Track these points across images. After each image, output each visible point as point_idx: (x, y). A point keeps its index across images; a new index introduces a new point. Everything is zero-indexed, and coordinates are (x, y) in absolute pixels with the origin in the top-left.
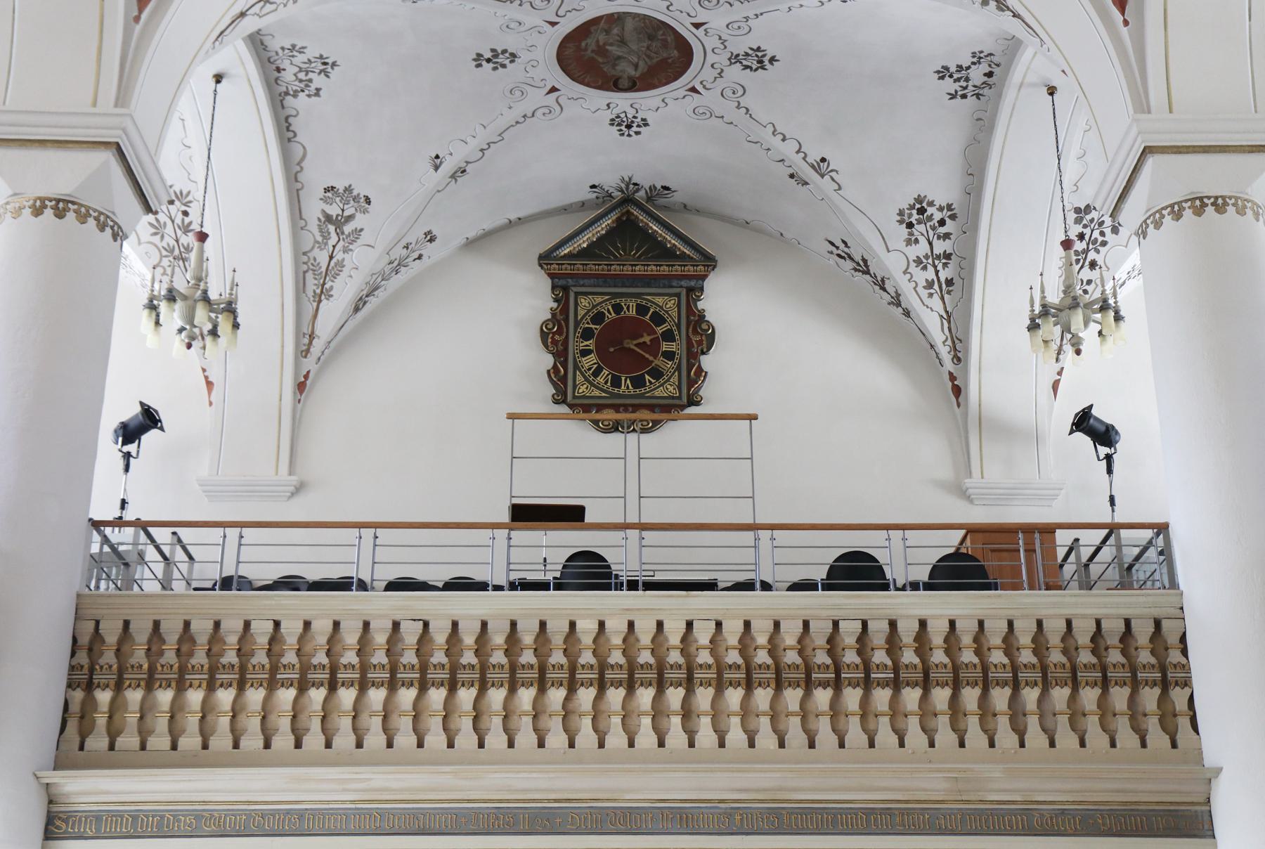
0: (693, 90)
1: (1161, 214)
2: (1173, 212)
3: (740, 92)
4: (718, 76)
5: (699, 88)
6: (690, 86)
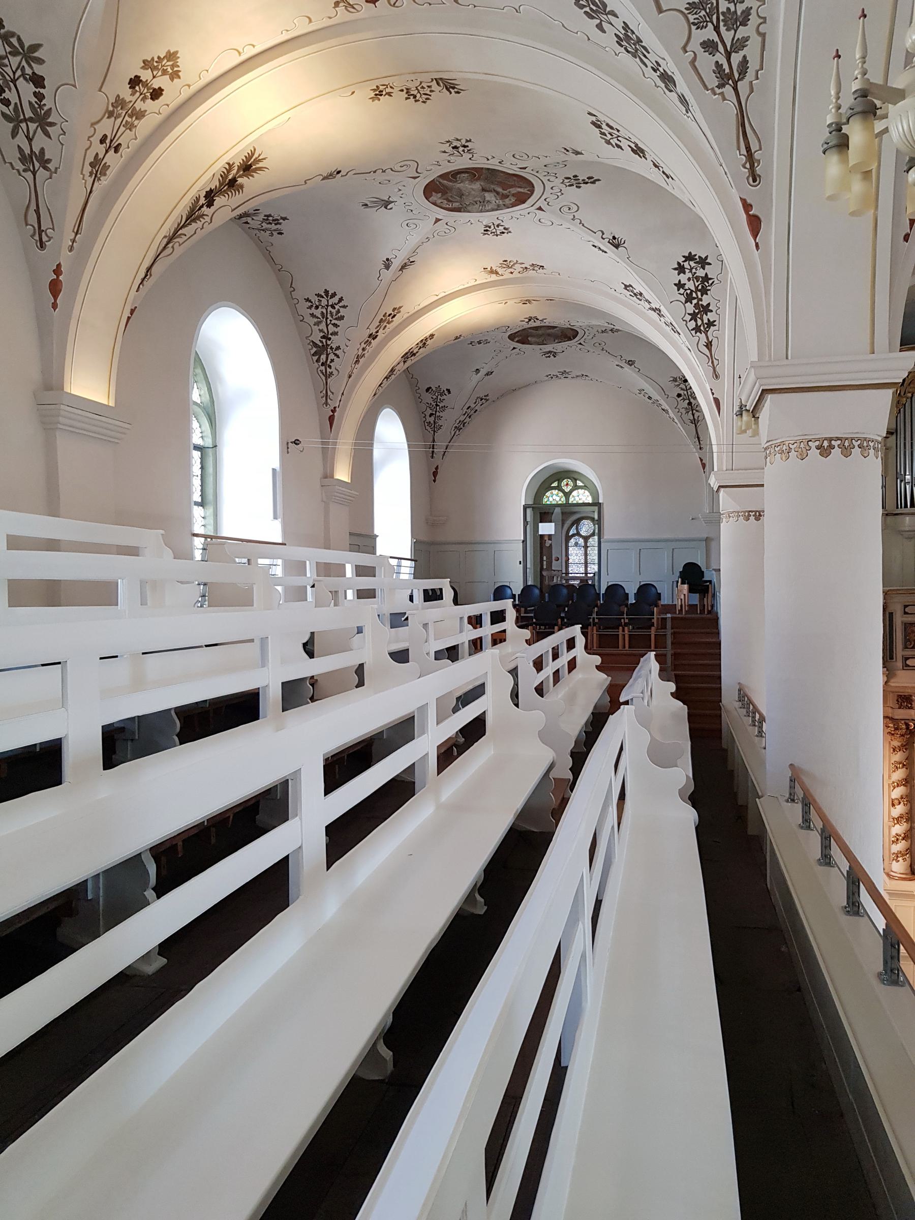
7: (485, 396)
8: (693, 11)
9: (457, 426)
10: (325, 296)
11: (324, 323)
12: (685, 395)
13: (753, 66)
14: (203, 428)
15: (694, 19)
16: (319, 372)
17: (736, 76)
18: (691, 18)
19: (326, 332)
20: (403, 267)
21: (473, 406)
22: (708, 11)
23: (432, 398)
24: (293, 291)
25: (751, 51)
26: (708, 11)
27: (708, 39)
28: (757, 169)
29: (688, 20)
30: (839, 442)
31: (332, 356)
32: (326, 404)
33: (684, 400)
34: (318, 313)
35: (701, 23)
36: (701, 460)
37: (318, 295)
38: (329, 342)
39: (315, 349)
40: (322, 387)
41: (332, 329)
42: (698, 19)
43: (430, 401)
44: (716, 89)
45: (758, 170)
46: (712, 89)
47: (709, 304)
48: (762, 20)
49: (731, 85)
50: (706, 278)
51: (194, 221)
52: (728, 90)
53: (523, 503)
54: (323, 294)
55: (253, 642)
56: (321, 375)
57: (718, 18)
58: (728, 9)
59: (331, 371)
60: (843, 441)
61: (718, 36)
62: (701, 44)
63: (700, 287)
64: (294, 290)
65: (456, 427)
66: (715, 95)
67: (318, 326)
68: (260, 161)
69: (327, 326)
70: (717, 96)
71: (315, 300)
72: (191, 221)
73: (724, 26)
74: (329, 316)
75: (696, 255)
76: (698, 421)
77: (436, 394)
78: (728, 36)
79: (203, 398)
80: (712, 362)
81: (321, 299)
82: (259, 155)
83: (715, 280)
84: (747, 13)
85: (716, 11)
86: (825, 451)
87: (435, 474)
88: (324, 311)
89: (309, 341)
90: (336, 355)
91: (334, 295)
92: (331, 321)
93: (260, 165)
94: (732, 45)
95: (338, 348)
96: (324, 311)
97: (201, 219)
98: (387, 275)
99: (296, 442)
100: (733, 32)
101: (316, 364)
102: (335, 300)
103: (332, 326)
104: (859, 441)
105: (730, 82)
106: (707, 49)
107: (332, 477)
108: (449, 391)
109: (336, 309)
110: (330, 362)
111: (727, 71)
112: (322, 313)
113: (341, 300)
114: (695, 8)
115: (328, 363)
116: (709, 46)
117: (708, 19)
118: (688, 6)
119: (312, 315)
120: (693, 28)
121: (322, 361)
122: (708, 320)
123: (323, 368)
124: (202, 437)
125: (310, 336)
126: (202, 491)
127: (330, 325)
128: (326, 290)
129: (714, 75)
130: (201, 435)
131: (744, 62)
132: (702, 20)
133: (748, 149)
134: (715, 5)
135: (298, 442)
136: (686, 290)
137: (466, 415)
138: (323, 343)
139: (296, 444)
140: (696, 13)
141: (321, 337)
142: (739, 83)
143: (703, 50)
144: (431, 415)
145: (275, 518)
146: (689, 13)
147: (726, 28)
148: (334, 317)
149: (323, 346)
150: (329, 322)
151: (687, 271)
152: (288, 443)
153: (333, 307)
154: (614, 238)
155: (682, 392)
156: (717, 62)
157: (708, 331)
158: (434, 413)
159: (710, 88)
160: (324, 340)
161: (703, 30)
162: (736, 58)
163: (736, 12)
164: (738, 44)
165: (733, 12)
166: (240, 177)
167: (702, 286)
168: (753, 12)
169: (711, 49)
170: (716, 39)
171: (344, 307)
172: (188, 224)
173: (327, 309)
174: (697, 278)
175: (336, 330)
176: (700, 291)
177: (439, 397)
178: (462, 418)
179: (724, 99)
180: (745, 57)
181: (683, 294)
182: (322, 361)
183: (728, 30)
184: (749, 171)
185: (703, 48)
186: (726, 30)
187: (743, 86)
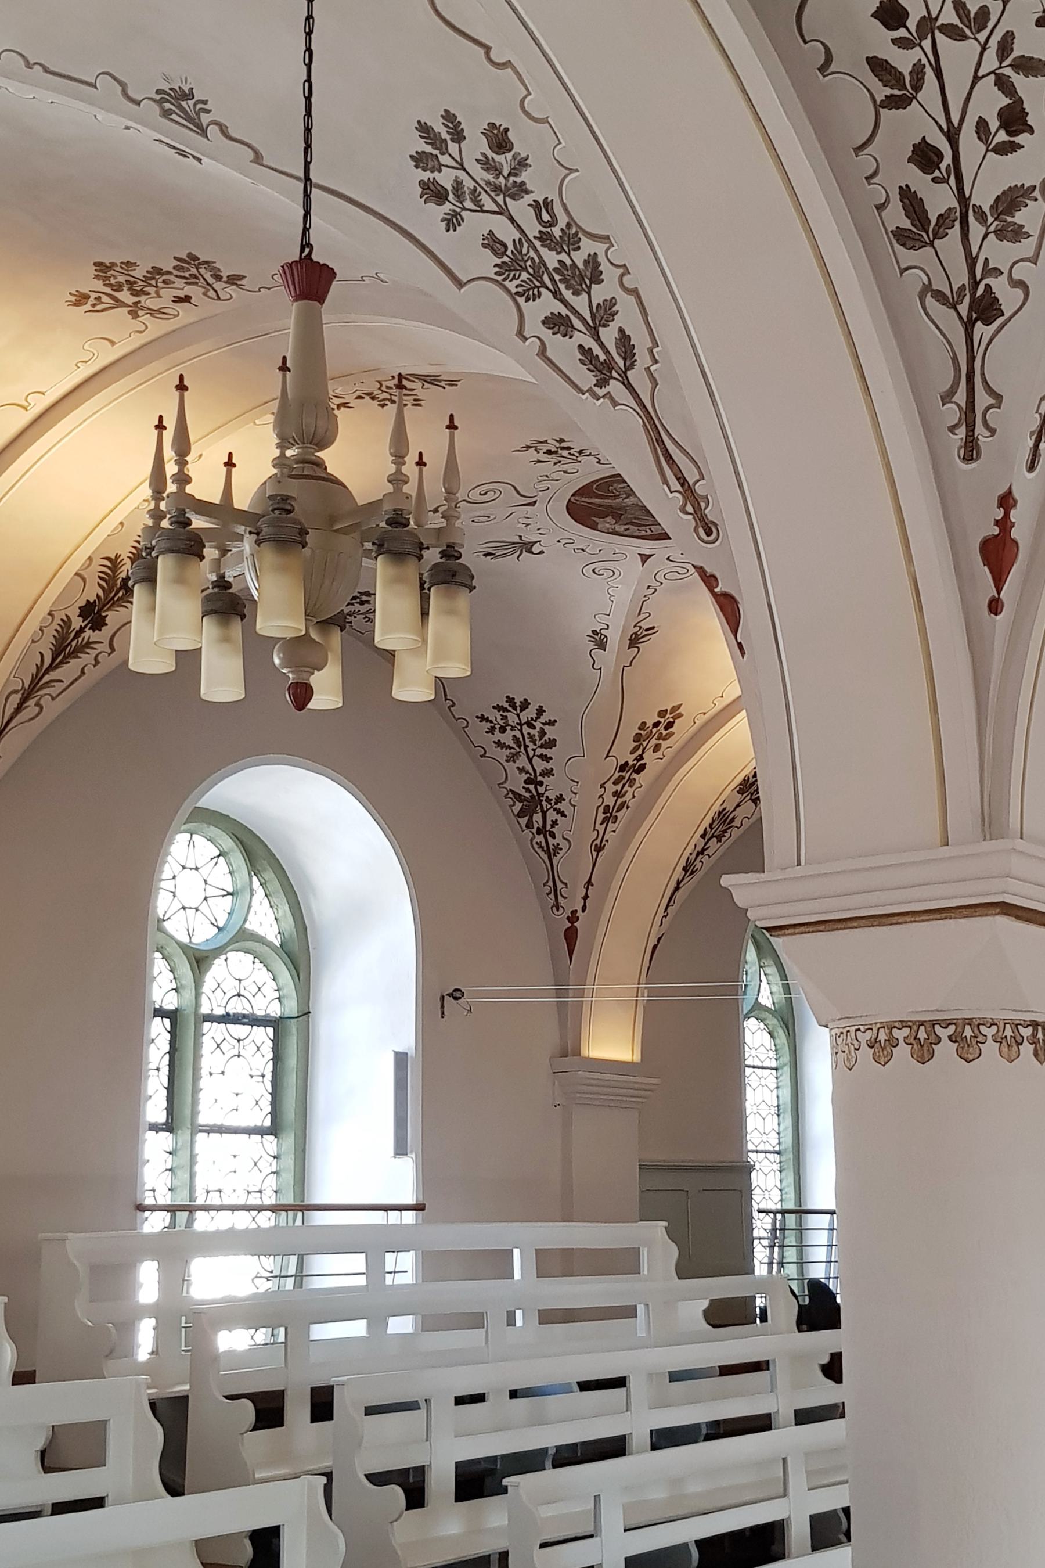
8: (509, 275)
10: (510, 708)
11: (524, 757)
14: (281, 981)
15: (517, 287)
16: (536, 846)
17: (620, 362)
18: (512, 286)
19: (531, 771)
20: (635, 641)
22: (531, 271)
24: (452, 706)
25: (627, 317)
26: (531, 271)
27: (552, 313)
28: (706, 512)
30: (906, 1032)
31: (552, 815)
35: (528, 290)
37: (499, 708)
38: (541, 790)
41: (540, 765)
42: (522, 286)
44: (596, 389)
45: (710, 513)
46: (590, 390)
48: (621, 270)
49: (617, 379)
51: (74, 654)
52: (615, 387)
54: (506, 705)
55: (456, 1398)
56: (539, 851)
57: (552, 279)
59: (555, 842)
60: (915, 1028)
61: (566, 306)
62: (544, 323)
66: (598, 400)
67: (514, 762)
69: (530, 760)
70: (602, 400)
71: (495, 716)
72: (65, 657)
73: (567, 288)
78: (580, 303)
79: (283, 925)
81: (505, 714)
85: (543, 269)
86: (924, 1052)
88: (518, 734)
89: (505, 792)
90: (558, 811)
91: (525, 705)
92: (534, 750)
95: (560, 799)
96: (518, 734)
97: (88, 651)
98: (609, 658)
99: (457, 995)
100: (585, 296)
101: (527, 831)
102: (530, 713)
103: (540, 760)
104: (952, 1028)
105: (614, 374)
106: (556, 329)
107: (577, 1052)
109: (538, 729)
110: (552, 826)
111: (602, 357)
113: (540, 711)
114: (511, 270)
115: (548, 827)
116: (557, 323)
117: (538, 284)
118: (497, 269)
119: (499, 744)
120: (521, 300)
123: (540, 838)
124: (279, 999)
125: (505, 782)
126: (273, 1103)
127: (535, 757)
128: (508, 697)
129: (585, 367)
130: (276, 995)
131: (624, 338)
132: (529, 287)
133: (682, 480)
134: (537, 260)
135: (458, 994)
138: (530, 792)
139: (456, 998)
140: (514, 278)
141: (525, 782)
142: (629, 373)
143: (551, 331)
145: (401, 1149)
146: (505, 280)
147: (571, 291)
148: (538, 743)
149: (532, 797)
150: (531, 753)
152: (443, 998)
156: (581, 346)
159: (585, 389)
160: (532, 787)
161: (537, 300)
163: (574, 265)
164: (602, 312)
165: (570, 265)
168: (601, 259)
169: (562, 328)
170: (564, 311)
172: (62, 662)
173: (521, 731)
175: (548, 766)
179: (615, 403)
180: (621, 330)
182: (536, 826)
184: (694, 518)
185: (549, 328)
186: (573, 294)
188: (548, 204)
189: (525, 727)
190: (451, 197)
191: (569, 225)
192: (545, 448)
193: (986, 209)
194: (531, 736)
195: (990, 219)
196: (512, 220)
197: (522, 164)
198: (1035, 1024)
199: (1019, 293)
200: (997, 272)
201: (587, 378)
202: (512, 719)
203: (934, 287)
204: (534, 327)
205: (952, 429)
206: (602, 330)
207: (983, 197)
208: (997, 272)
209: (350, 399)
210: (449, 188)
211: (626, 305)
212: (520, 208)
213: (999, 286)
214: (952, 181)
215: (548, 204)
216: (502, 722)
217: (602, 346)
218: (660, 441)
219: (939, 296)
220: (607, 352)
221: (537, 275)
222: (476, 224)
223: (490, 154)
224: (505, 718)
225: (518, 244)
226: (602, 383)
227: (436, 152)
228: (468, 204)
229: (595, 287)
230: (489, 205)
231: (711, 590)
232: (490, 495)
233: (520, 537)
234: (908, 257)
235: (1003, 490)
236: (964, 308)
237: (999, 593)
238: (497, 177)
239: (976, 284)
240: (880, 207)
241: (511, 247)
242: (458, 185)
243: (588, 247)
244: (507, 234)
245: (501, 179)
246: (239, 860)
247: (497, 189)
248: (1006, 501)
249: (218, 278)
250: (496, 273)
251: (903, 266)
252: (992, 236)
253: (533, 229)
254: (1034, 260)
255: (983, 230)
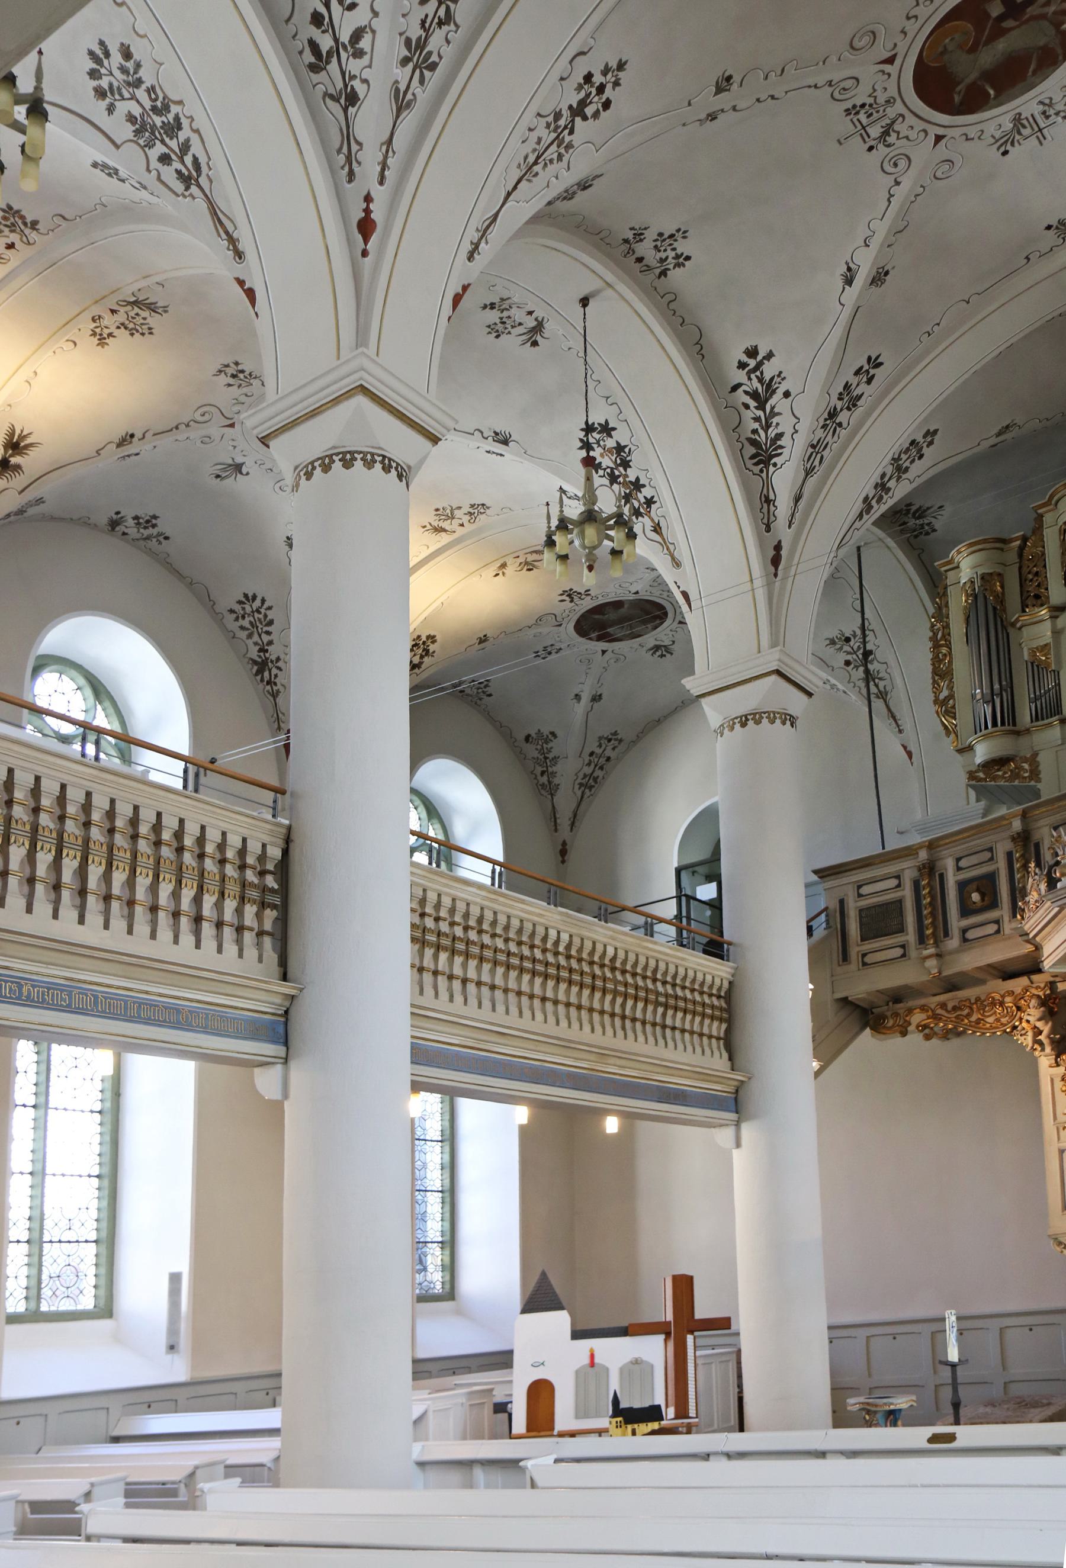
0: (890, 61)
1: (746, 717)
2: (740, 722)
3: (836, 95)
4: (874, 94)
5: (887, 68)
6: (898, 62)
7: (612, 734)
9: (584, 781)
12: (856, 660)
13: (203, 160)
17: (194, 174)
18: (141, 142)
21: (599, 751)
23: (537, 749)
25: (196, 148)
29: (139, 144)
31: (274, 671)
32: (279, 728)
33: (857, 667)
34: (246, 623)
36: (905, 747)
37: (240, 602)
38: (267, 655)
39: (256, 668)
40: (271, 710)
41: (266, 638)
43: (536, 754)
45: (240, 247)
47: (638, 479)
50: (620, 448)
52: (194, 189)
53: (676, 865)
54: (244, 600)
56: (268, 696)
58: (163, 122)
63: (619, 461)
64: (214, 604)
65: (581, 785)
68: (25, 436)
69: (260, 635)
71: (237, 608)
74: (258, 624)
75: (593, 424)
76: (886, 695)
77: (540, 743)
78: (173, 144)
80: (668, 549)
82: (22, 431)
83: (631, 446)
84: (177, 118)
87: (563, 852)
91: (254, 597)
93: (28, 441)
94: (180, 150)
95: (278, 659)
96: (252, 620)
100: (175, 139)
102: (257, 603)
104: (341, 456)
105: (193, 182)
108: (553, 734)
111: (186, 173)
112: (251, 623)
113: (263, 601)
116: (165, 159)
119: (242, 628)
120: (146, 149)
121: (266, 680)
122: (645, 497)
123: (268, 688)
131: (196, 160)
133: (227, 233)
136: (605, 469)
137: (593, 766)
144: (543, 773)
148: (264, 623)
150: (260, 631)
151: (595, 446)
153: (259, 612)
154: (496, 434)
155: (849, 657)
156: (176, 170)
157: (650, 512)
158: (545, 769)
160: (262, 654)
162: (188, 159)
163: (169, 122)
166: (11, 456)
167: (620, 459)
168: (181, 115)
171: (270, 608)
174: (610, 451)
176: (620, 465)
177: (545, 745)
178: (588, 770)
179: (194, 198)
180: (194, 156)
181: (604, 476)
182: (266, 680)
183: (171, 139)
187: (203, 180)
188: (153, 88)
189: (256, 614)
190: (109, 94)
191: (164, 99)
192: (230, 371)
193: (347, 43)
194: (259, 620)
195: (349, 48)
196: (138, 101)
197: (138, 66)
198: (384, 457)
199: (365, 86)
200: (355, 77)
201: (179, 187)
202: (248, 609)
203: (329, 92)
204: (155, 164)
205: (342, 168)
206: (185, 158)
207: (345, 37)
208: (355, 77)
209: (113, 329)
210: (107, 88)
211: (195, 140)
212: (141, 93)
213: (356, 84)
214: (330, 30)
215: (153, 88)
216: (242, 612)
217: (186, 167)
218: (216, 214)
219: (332, 97)
220: (188, 169)
221: (153, 133)
222: (124, 107)
223: (123, 63)
224: (243, 609)
225: (142, 116)
226: (187, 188)
227: (98, 67)
228: (117, 97)
229: (180, 133)
230: (126, 95)
231: (242, 287)
232: (207, 417)
233: (233, 459)
234: (315, 78)
235: (365, 193)
236: (342, 101)
237: (366, 245)
238: (128, 76)
239: (346, 86)
240: (301, 53)
241: (139, 119)
242: (111, 86)
243: (174, 109)
244: (137, 111)
245: (130, 77)
246: (88, 691)
247: (129, 84)
248: (368, 199)
249: (25, 224)
250: (135, 136)
251: (314, 83)
252: (351, 58)
253: (148, 104)
254: (370, 66)
255: (346, 55)
